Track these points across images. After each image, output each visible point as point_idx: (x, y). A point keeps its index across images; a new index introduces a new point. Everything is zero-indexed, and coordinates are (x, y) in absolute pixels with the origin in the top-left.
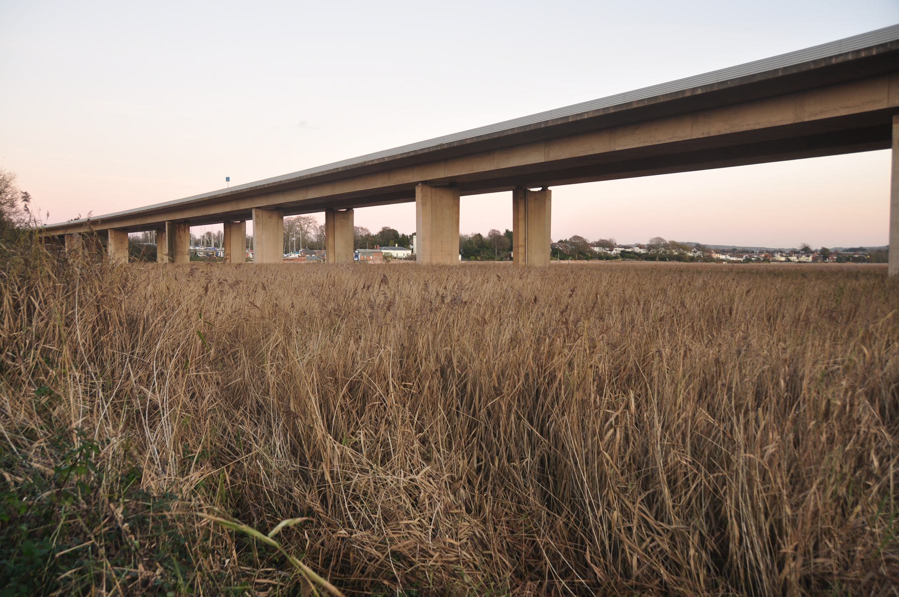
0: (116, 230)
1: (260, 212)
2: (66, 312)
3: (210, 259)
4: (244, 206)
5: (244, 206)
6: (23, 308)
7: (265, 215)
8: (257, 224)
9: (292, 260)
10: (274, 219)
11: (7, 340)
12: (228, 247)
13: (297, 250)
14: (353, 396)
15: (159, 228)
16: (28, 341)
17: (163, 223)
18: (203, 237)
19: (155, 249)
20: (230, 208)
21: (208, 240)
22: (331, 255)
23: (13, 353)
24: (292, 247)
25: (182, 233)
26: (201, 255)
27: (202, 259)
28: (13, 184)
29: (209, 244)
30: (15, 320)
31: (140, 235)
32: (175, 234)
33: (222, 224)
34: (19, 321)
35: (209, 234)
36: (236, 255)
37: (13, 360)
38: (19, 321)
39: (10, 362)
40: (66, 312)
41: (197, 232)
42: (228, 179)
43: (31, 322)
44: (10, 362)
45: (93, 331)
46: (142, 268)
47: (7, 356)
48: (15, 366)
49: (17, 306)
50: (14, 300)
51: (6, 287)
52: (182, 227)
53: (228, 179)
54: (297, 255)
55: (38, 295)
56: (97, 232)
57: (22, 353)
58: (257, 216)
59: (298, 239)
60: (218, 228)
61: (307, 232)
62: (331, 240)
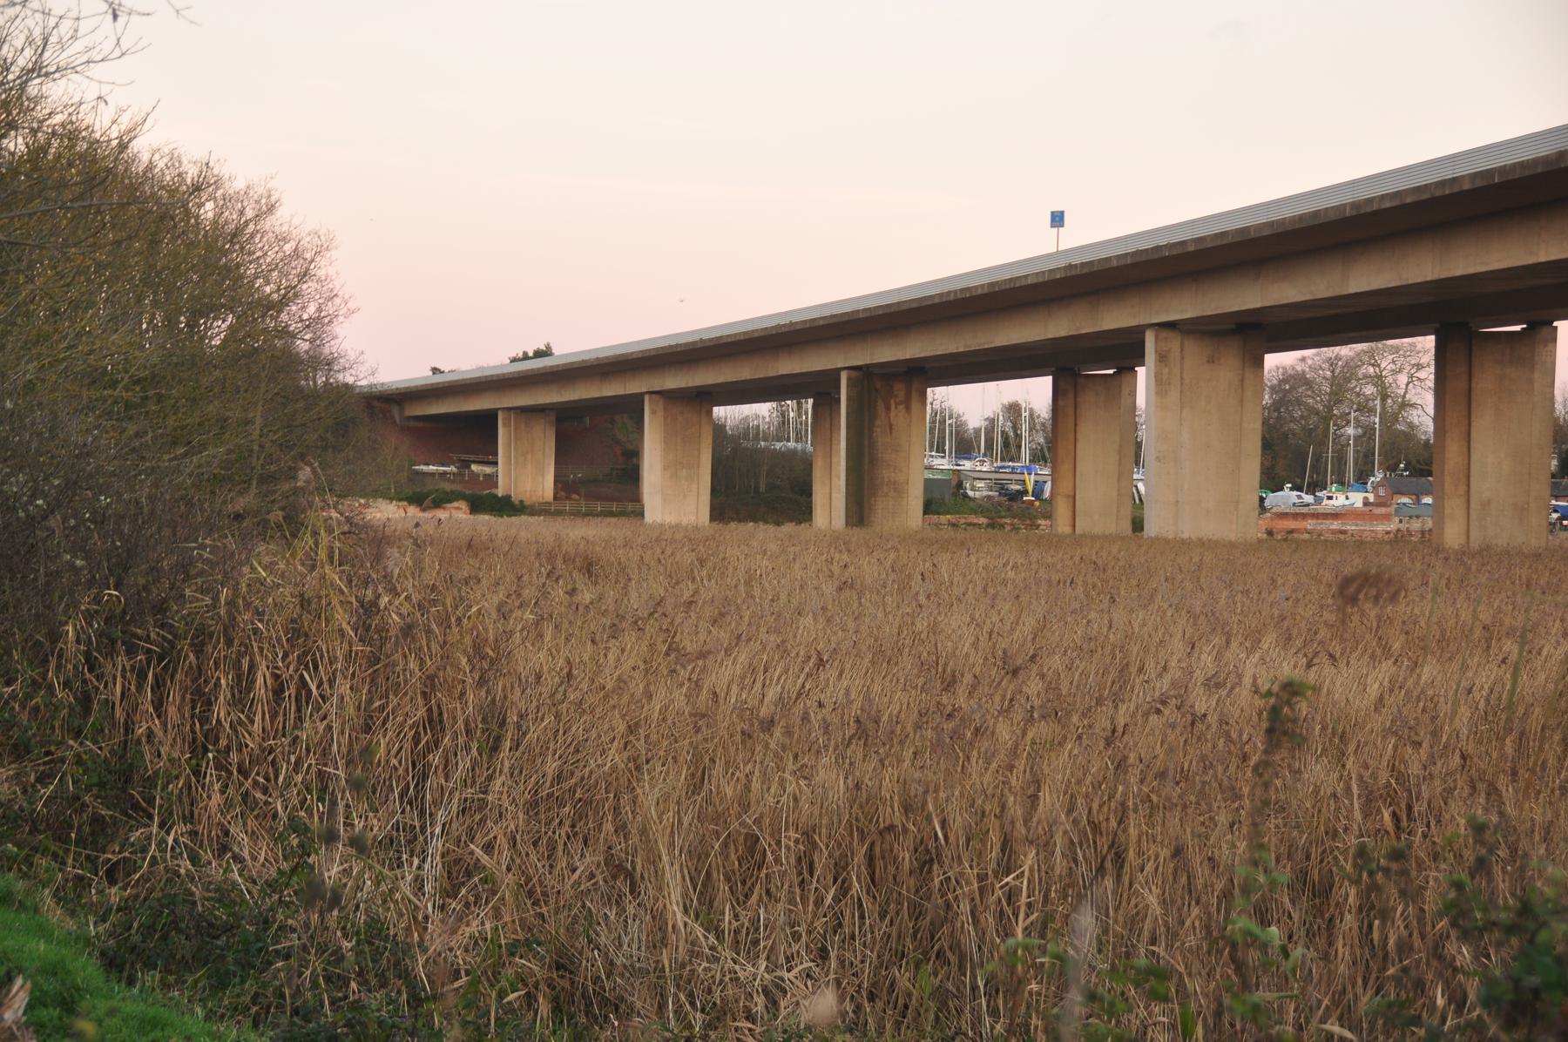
0: (670, 397)
1: (1174, 343)
2: (370, 701)
3: (1012, 509)
4: (1114, 318)
5: (1114, 318)
6: (290, 692)
7: (1193, 353)
8: (1160, 385)
9: (1335, 516)
10: (1227, 371)
11: (257, 751)
12: (1065, 468)
13: (1362, 479)
14: (736, 863)
15: (821, 388)
16: (293, 759)
17: (832, 376)
18: (992, 421)
19: (807, 464)
20: (1075, 321)
21: (1003, 439)
22: (1454, 506)
23: (267, 779)
24: (1340, 460)
25: (898, 415)
26: (978, 490)
27: (978, 507)
28: (322, 269)
29: (1010, 448)
30: (274, 716)
31: (762, 412)
32: (873, 416)
33: (1047, 381)
34: (281, 718)
35: (1013, 410)
36: (1093, 502)
37: (265, 791)
38: (281, 718)
39: (258, 795)
40: (370, 701)
41: (972, 403)
42: (1057, 219)
43: (300, 719)
44: (258, 795)
45: (416, 745)
46: (757, 544)
47: (256, 783)
48: (266, 803)
49: (278, 692)
50: (276, 677)
51: (261, 649)
52: (899, 389)
53: (1057, 219)
54: (1356, 499)
55: (316, 668)
56: (592, 414)
57: (281, 779)
58: (1162, 358)
59: (1368, 432)
60: (1036, 392)
61: (1405, 405)
62: (1453, 451)
